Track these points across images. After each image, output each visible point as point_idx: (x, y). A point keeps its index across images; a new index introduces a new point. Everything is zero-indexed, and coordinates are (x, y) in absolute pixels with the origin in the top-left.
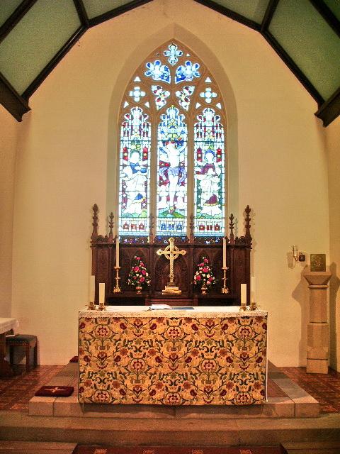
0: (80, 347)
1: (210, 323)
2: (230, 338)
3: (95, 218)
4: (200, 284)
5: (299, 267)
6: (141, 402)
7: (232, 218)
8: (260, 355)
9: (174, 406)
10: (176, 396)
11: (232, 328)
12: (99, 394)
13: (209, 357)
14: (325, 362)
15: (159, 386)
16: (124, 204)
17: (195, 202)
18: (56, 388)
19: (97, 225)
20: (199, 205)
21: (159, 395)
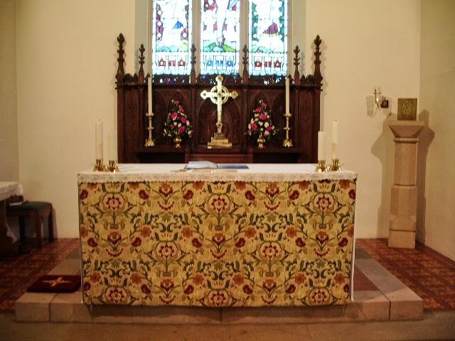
0: (82, 225)
1: (272, 190)
2: (302, 211)
3: (121, 52)
4: (256, 136)
5: (381, 115)
6: (173, 303)
7: (297, 51)
8: (345, 235)
9: (221, 308)
10: (223, 295)
11: (305, 196)
12: (111, 292)
13: (271, 239)
14: (412, 233)
15: (198, 280)
16: (159, 35)
17: (250, 32)
18: (60, 279)
19: (123, 60)
20: (255, 36)
21: (198, 293)
